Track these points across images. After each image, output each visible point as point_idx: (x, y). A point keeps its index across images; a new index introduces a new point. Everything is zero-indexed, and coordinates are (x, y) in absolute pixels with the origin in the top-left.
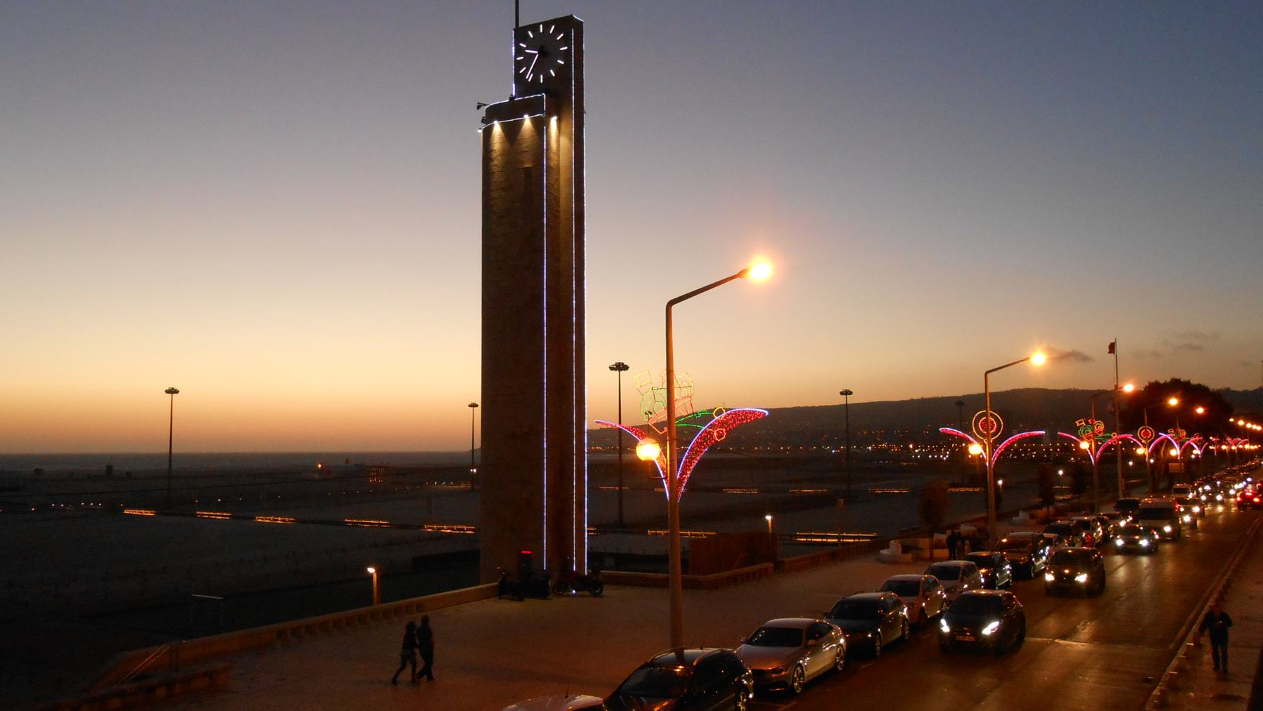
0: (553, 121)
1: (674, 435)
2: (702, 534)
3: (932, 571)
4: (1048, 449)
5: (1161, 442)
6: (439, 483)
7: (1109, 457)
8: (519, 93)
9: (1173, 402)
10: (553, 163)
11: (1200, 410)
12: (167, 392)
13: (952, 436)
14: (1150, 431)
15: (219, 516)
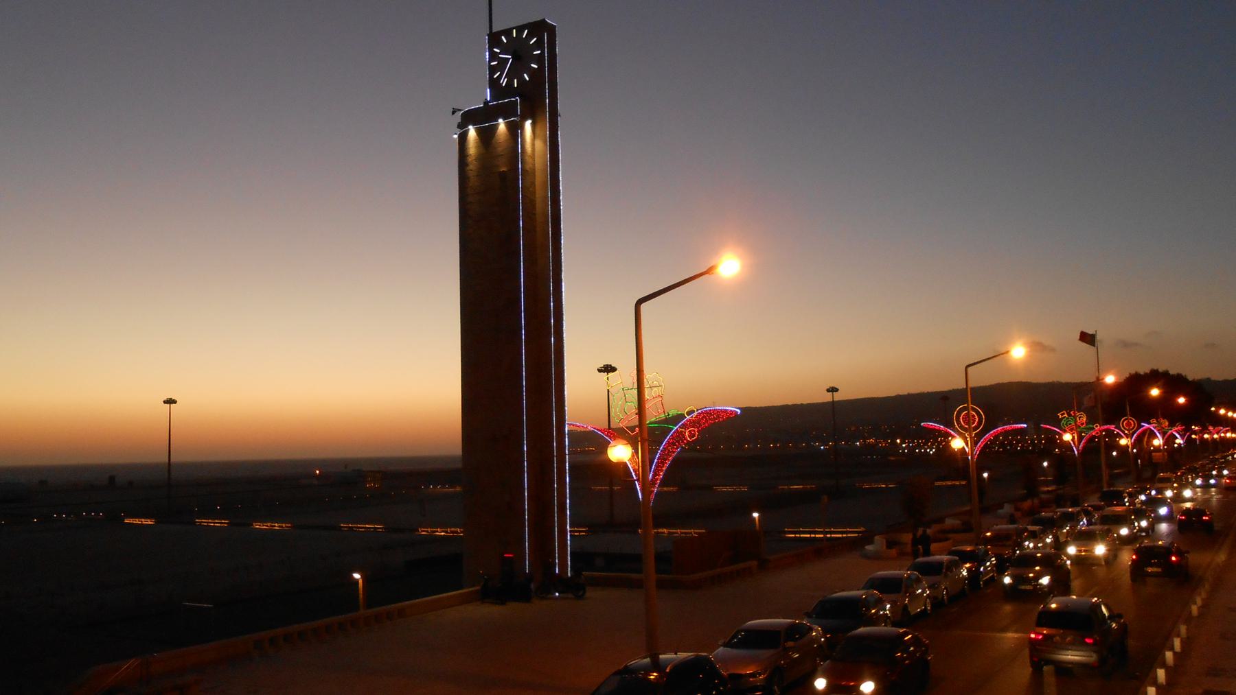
0: (528, 124)
1: (646, 435)
2: (693, 532)
3: (915, 567)
4: (1033, 442)
5: (1144, 433)
6: (435, 486)
7: (1093, 449)
8: (493, 97)
9: (1155, 392)
10: (528, 167)
11: (1182, 400)
12: (828, 390)
13: (939, 431)
14: (1133, 421)
15: (217, 523)
